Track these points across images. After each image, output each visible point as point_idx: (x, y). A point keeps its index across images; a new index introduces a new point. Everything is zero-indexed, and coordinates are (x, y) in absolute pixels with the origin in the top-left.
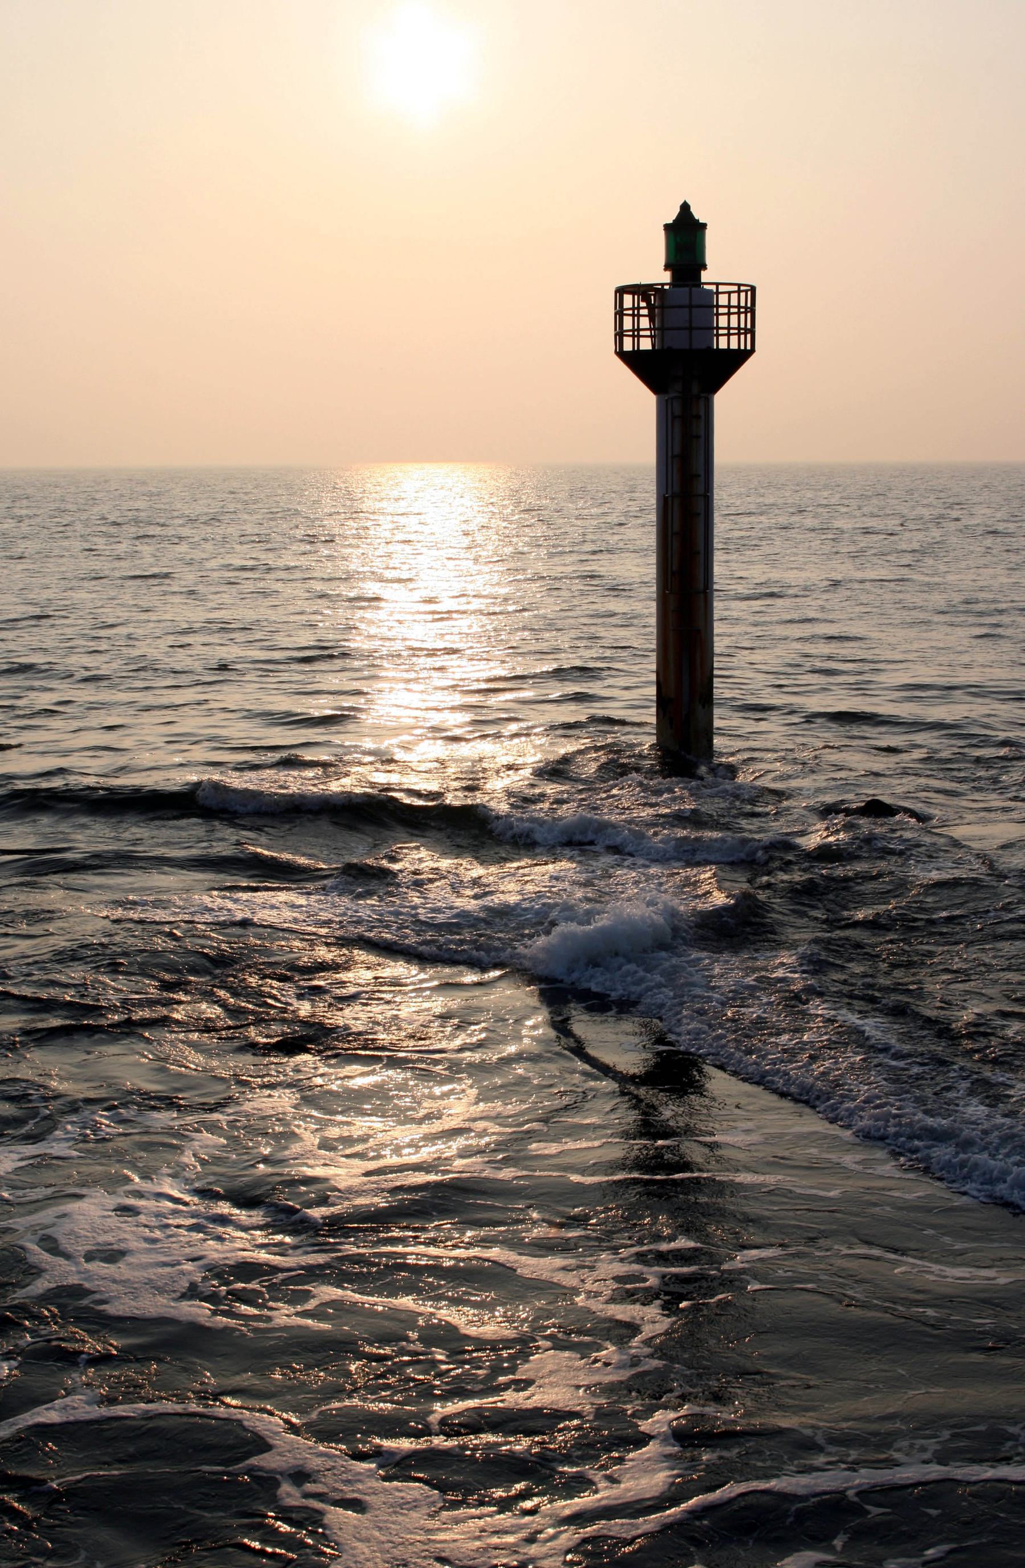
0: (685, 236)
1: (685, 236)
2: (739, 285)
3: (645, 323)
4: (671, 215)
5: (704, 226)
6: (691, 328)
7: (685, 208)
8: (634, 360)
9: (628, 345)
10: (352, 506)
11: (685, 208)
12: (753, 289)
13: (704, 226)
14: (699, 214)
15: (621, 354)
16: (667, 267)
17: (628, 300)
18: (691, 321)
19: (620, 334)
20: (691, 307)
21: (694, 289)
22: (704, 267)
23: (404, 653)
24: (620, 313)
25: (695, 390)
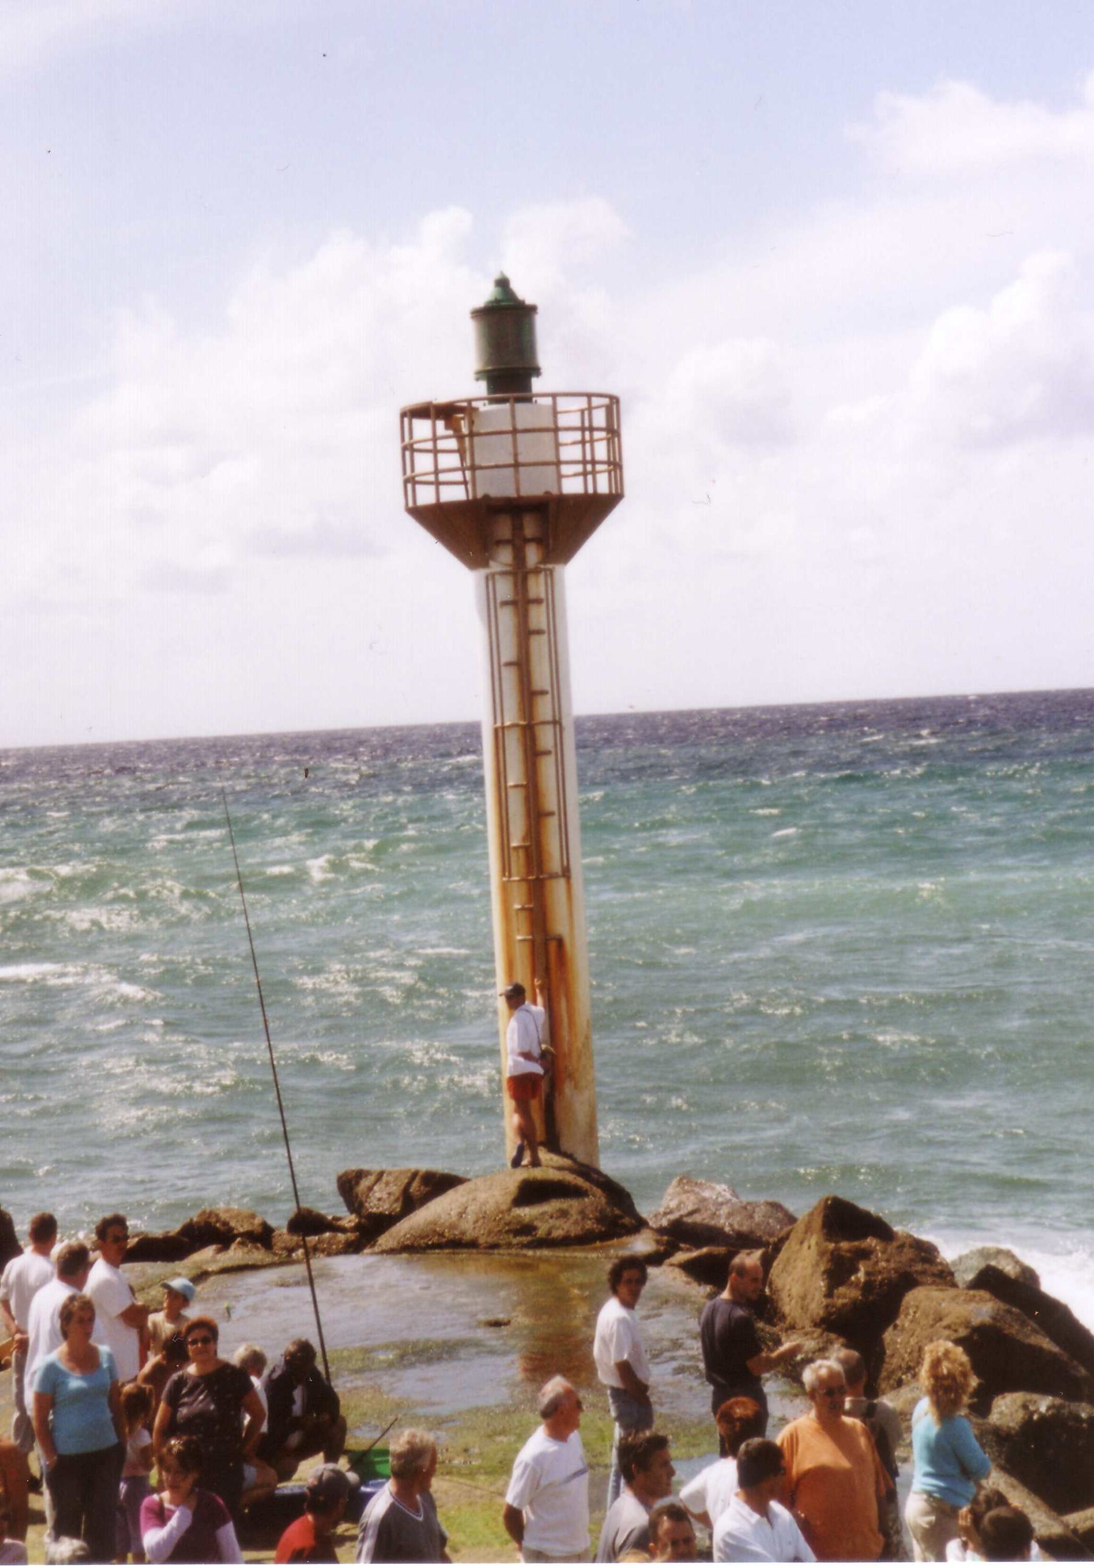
0: (507, 326)
1: (507, 326)
2: (589, 396)
3: (451, 460)
4: (485, 294)
5: (532, 309)
6: (516, 465)
7: (503, 283)
8: (440, 520)
9: (426, 496)
10: (837, 757)
11: (503, 283)
12: (614, 400)
13: (532, 309)
14: (524, 292)
15: (421, 514)
16: (481, 374)
17: (422, 428)
18: (516, 455)
19: (411, 481)
20: (515, 431)
21: (519, 407)
22: (536, 371)
23: (670, 966)
24: (409, 448)
25: (532, 555)
